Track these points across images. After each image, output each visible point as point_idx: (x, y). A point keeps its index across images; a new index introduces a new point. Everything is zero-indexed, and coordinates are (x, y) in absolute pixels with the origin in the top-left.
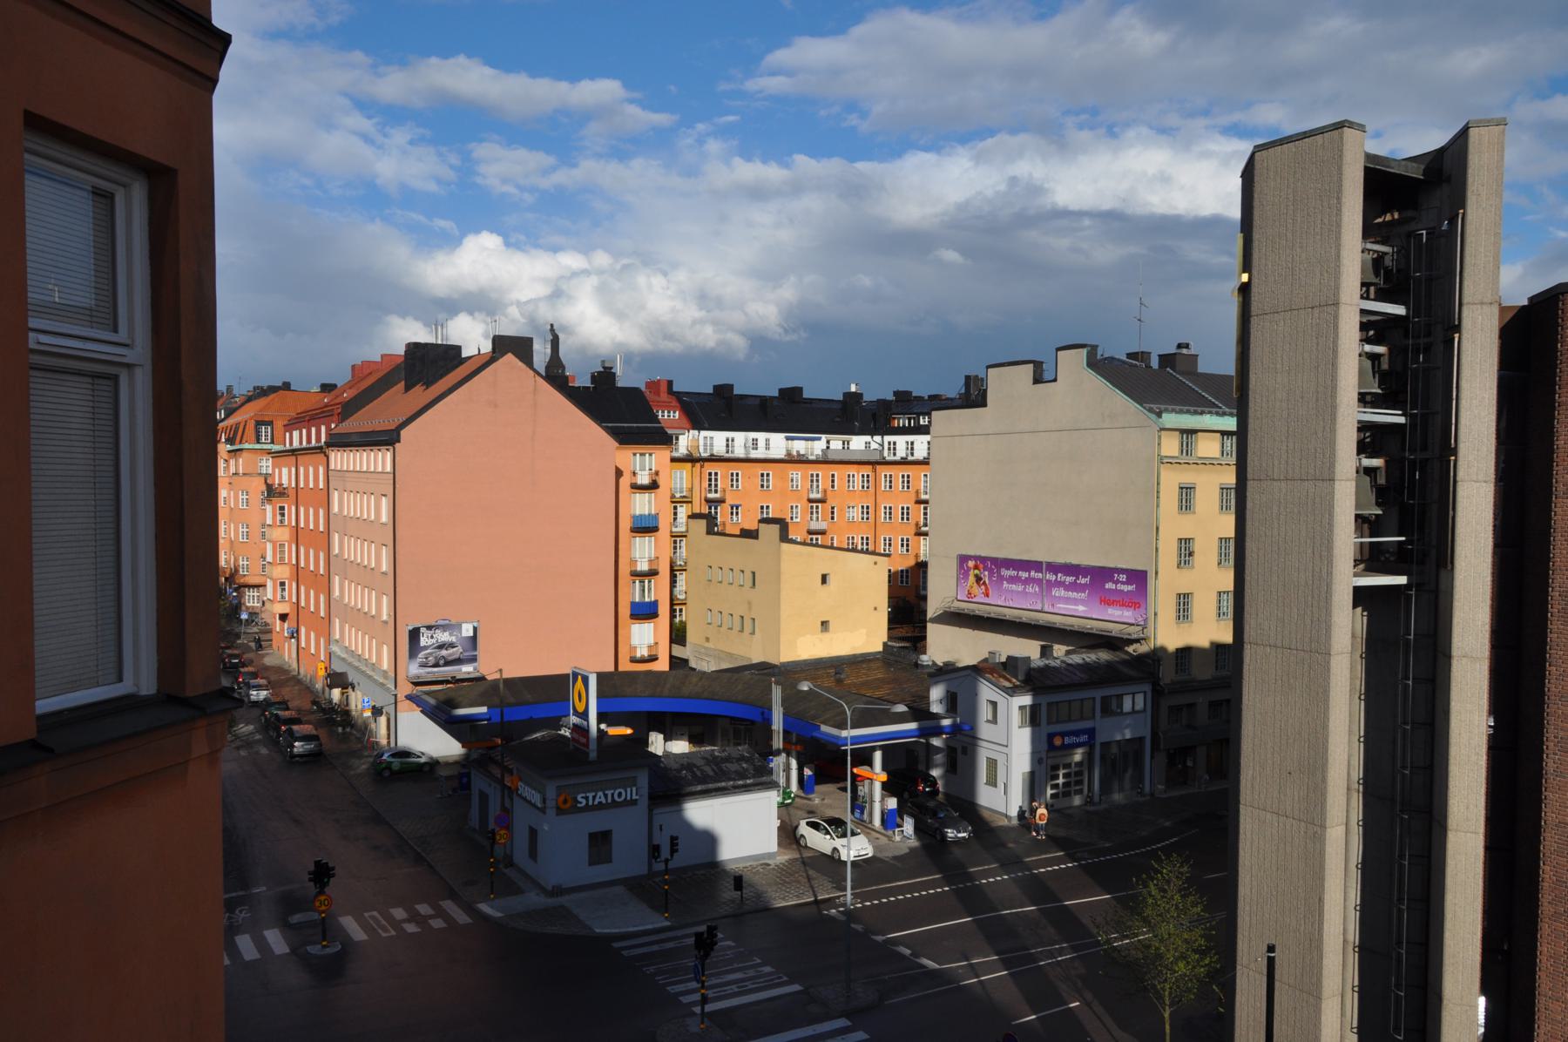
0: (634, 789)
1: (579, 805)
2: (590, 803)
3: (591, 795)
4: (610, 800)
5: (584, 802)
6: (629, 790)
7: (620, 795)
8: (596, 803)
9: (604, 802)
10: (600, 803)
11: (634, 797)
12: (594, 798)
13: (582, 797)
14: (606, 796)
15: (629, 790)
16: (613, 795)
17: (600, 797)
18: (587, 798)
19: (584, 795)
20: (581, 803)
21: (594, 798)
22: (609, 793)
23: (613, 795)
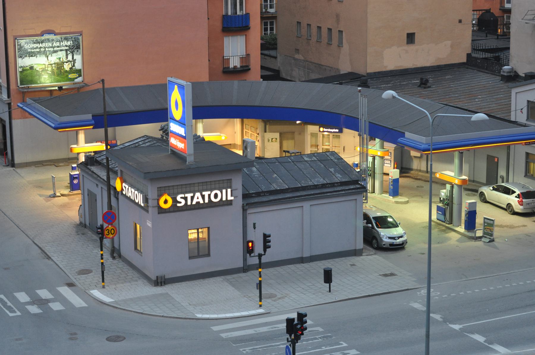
0: (229, 191)
1: (179, 205)
2: (189, 203)
3: (189, 196)
4: (207, 201)
5: (183, 202)
6: (224, 191)
7: (216, 196)
8: (194, 203)
9: (202, 202)
10: (198, 203)
11: (230, 198)
12: (192, 198)
13: (181, 198)
14: (203, 197)
15: (224, 191)
16: (209, 195)
17: (198, 198)
18: (186, 199)
19: (183, 196)
20: (180, 203)
21: (192, 198)
22: (206, 194)
23: (209, 195)
